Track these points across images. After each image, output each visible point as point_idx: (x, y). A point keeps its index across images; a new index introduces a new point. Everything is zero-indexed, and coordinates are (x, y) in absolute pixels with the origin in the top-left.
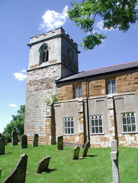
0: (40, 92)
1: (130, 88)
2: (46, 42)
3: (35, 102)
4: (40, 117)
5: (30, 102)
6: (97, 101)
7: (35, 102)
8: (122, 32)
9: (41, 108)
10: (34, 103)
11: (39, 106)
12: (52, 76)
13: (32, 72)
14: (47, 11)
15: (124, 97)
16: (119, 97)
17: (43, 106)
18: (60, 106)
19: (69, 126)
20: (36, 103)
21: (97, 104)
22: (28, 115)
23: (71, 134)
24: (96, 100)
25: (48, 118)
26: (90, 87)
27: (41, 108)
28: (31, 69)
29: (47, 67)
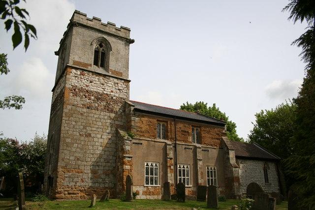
0: (93, 111)
1: (212, 142)
2: (110, 39)
3: (85, 127)
4: (93, 154)
5: (74, 123)
6: (185, 148)
7: (85, 127)
8: (259, 112)
9: (95, 139)
10: (82, 127)
11: (92, 135)
12: (117, 95)
13: (79, 72)
14: (268, 112)
15: (209, 149)
16: (206, 149)
17: (99, 136)
18: (141, 144)
19: (152, 174)
20: (86, 129)
21: (185, 152)
22: (67, 146)
23: (154, 185)
24: (184, 146)
25: (128, 159)
26: (177, 130)
27: (95, 139)
28: (74, 66)
29: (107, 77)
